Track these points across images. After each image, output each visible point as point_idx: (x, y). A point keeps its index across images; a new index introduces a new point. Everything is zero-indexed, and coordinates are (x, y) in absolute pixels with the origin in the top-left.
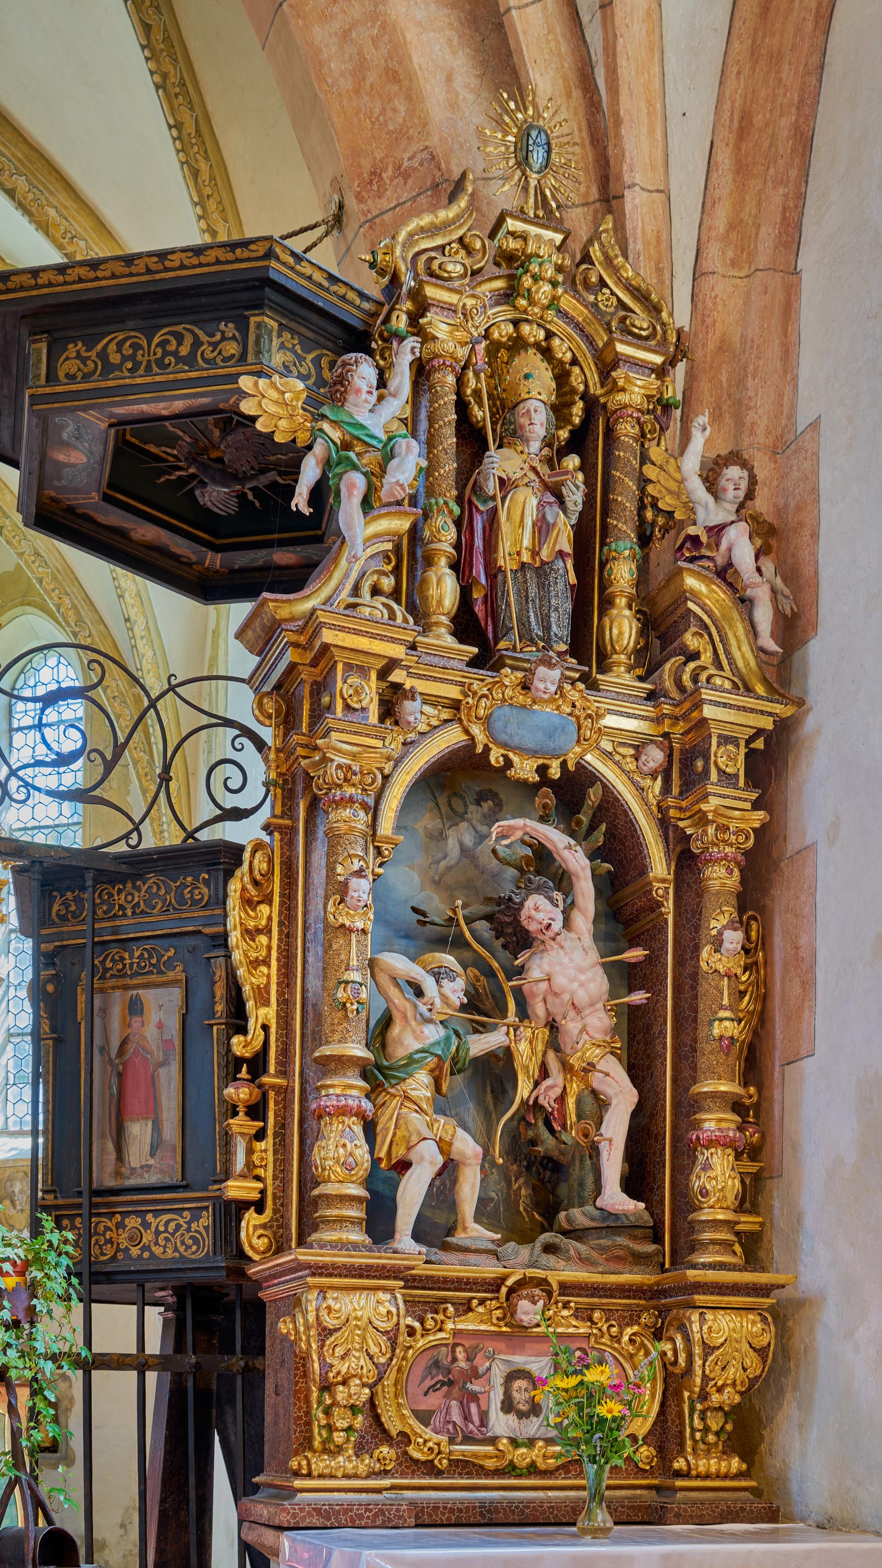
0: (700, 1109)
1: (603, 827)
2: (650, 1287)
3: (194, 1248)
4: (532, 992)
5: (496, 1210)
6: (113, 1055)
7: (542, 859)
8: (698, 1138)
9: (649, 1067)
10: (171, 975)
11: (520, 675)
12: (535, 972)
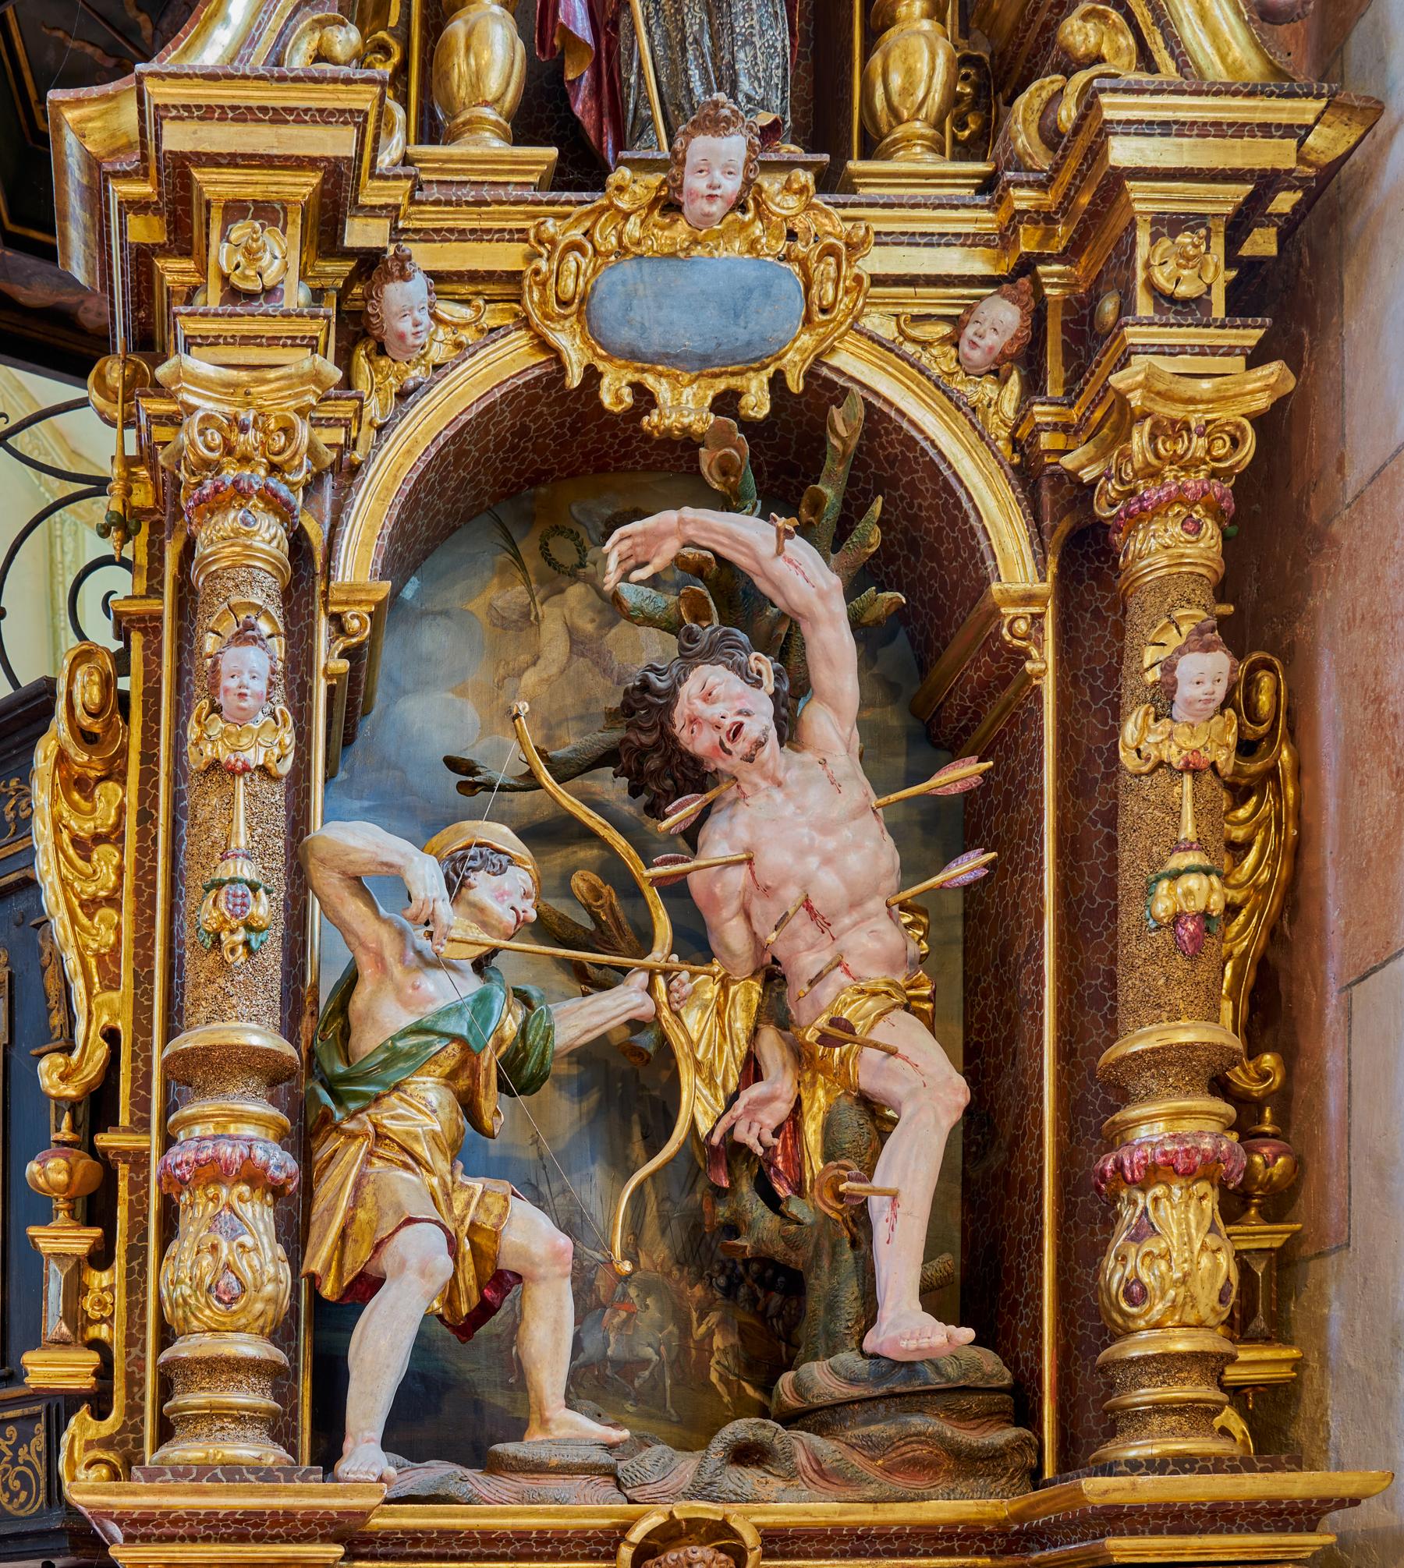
0: (1126, 1098)
1: (877, 507)
2: (1002, 1527)
4: (712, 896)
5: (655, 1383)
8: (1119, 1166)
11: (655, 179)
12: (717, 844)
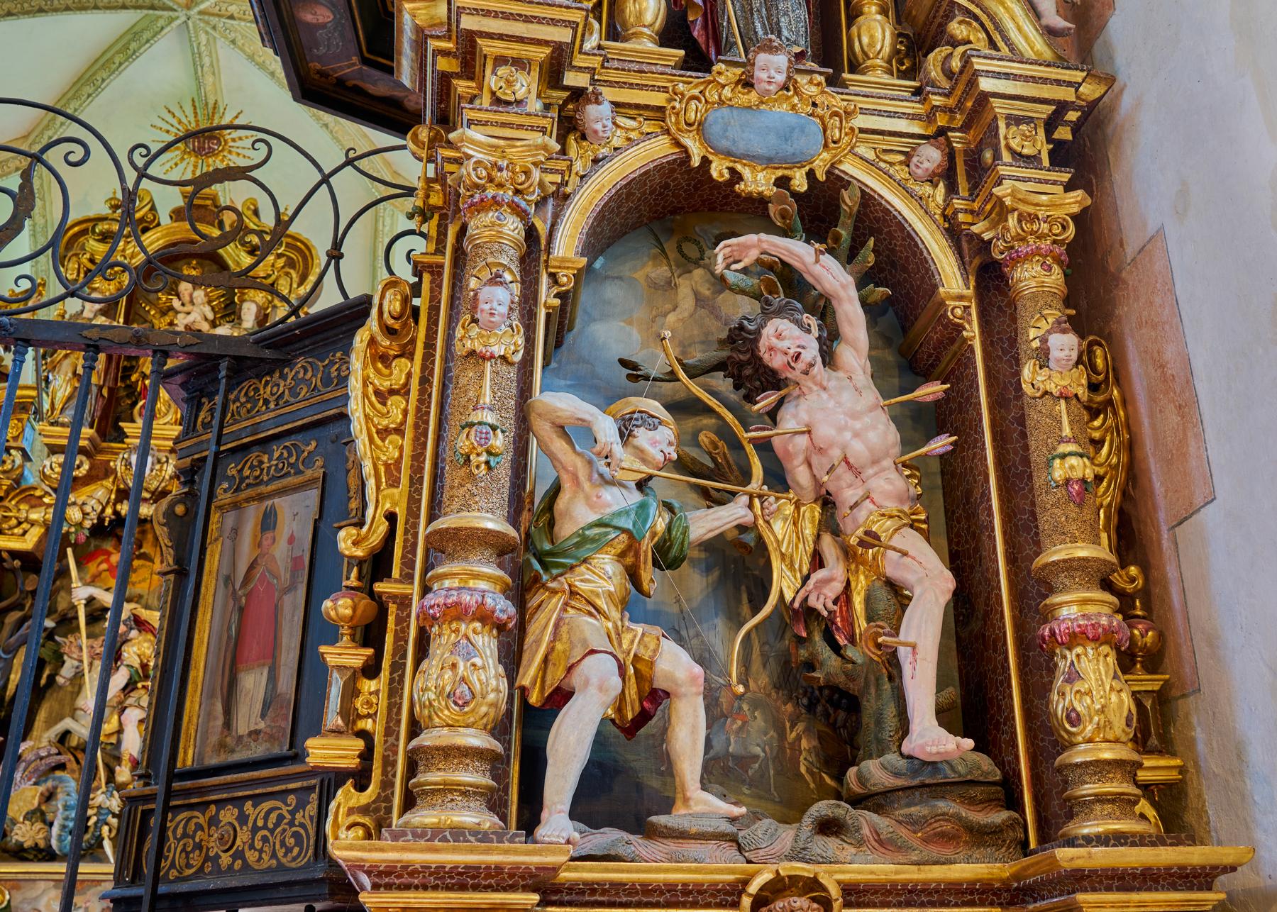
0: (1051, 590)
1: (871, 242)
2: (1006, 883)
3: (296, 850)
4: (787, 451)
5: (763, 773)
6: (237, 586)
7: (789, 285)
8: (1053, 633)
9: (977, 550)
10: (309, 473)
11: (739, 71)
